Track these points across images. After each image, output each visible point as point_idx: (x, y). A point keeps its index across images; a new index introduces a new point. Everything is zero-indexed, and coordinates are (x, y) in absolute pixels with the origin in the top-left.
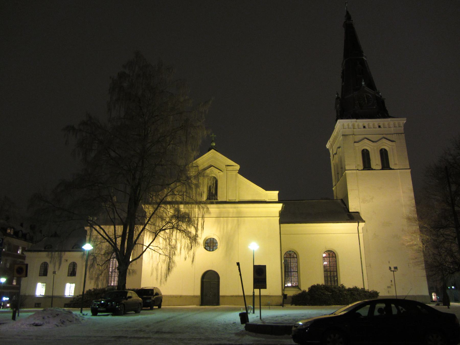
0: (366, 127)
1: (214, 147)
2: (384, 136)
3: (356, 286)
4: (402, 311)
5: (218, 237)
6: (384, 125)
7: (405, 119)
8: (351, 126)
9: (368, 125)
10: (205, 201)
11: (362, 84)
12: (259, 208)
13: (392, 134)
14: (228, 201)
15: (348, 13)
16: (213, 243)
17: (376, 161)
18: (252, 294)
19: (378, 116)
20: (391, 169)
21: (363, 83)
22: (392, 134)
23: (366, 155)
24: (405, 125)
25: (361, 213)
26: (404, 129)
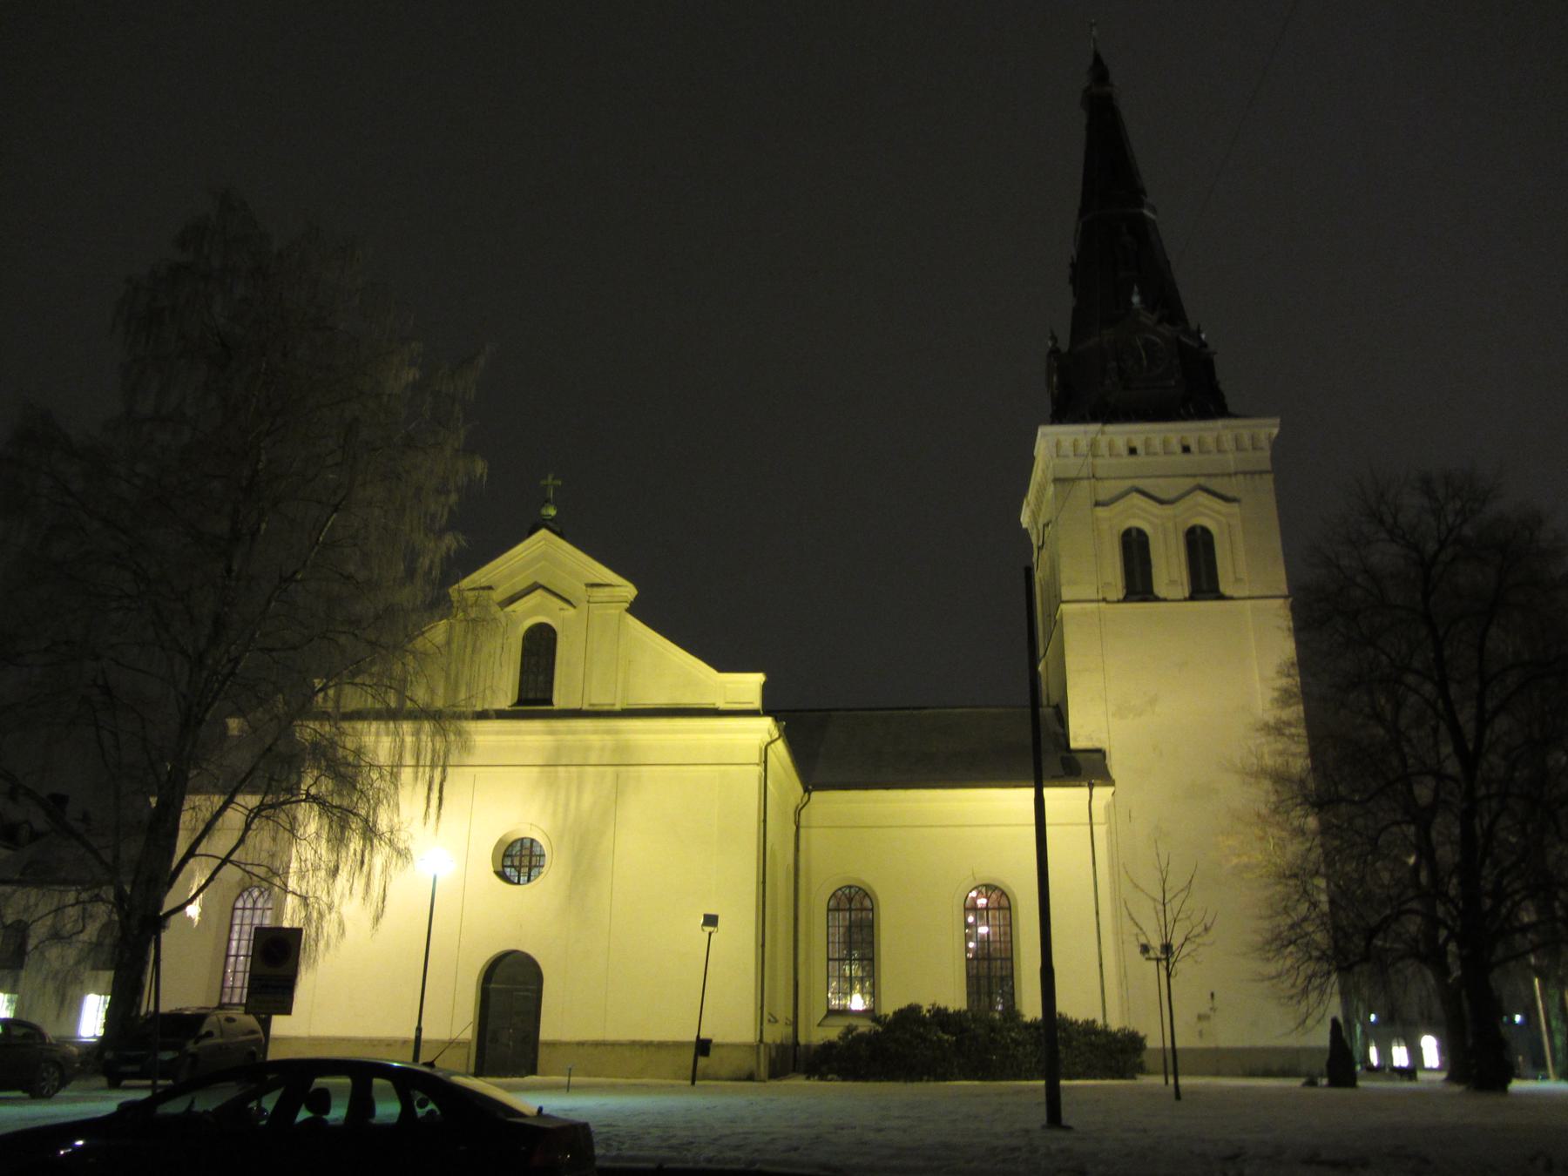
0: (1194, 447)
1: (551, 520)
2: (1202, 481)
4: (420, 1112)
5: (545, 834)
6: (1200, 442)
7: (1277, 421)
8: (1085, 448)
9: (1147, 443)
10: (510, 709)
11: (1131, 303)
12: (689, 731)
13: (1229, 475)
14: (585, 707)
15: (1098, 59)
16: (531, 855)
17: (1170, 569)
18: (412, 1035)
19: (1182, 411)
20: (1221, 597)
21: (1136, 299)
22: (1229, 475)
23: (1135, 548)
24: (1277, 445)
25: (1110, 752)
26: (1273, 459)
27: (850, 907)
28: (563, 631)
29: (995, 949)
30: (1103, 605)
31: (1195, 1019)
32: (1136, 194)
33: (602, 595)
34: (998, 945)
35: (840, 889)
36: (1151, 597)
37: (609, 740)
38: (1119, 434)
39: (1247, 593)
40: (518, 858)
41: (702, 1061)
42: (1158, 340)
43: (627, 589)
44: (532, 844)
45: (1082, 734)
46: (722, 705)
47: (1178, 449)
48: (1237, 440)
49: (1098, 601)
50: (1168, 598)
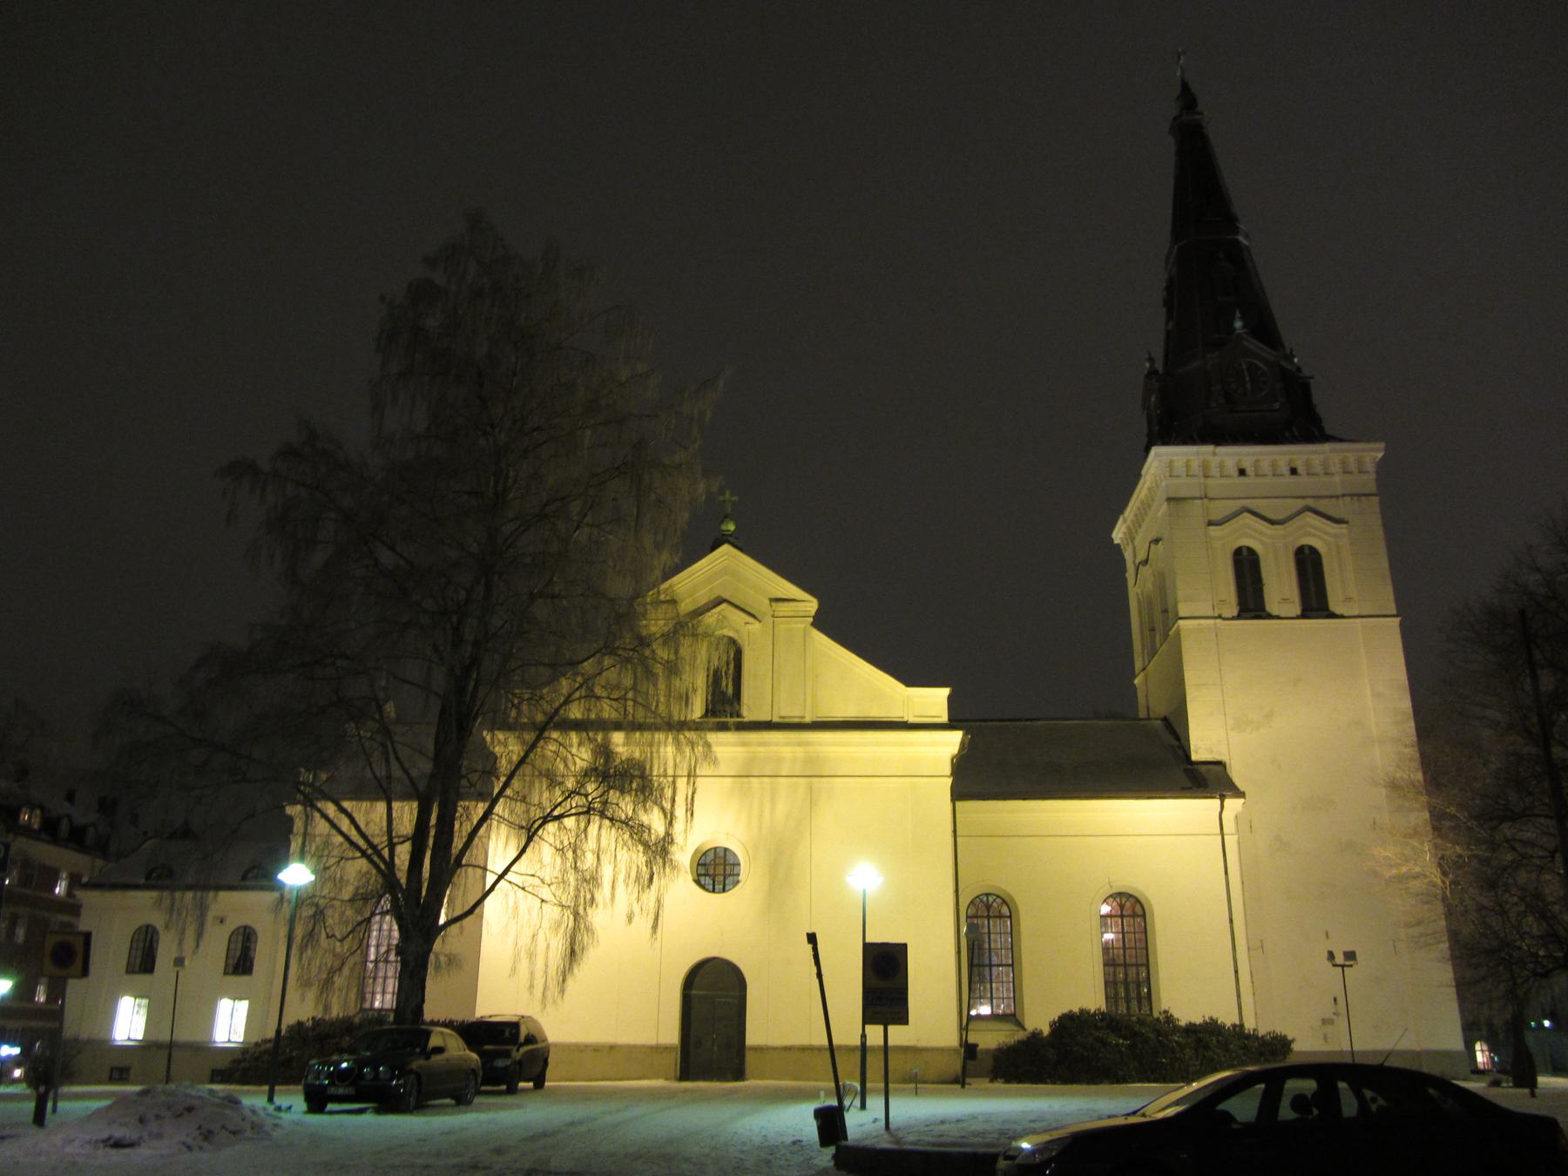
1: (730, 535)
2: (1310, 502)
3: (1214, 1017)
4: (1374, 1107)
7: (1382, 445)
13: (1337, 497)
14: (776, 719)
15: (1185, 87)
17: (1281, 587)
18: (858, 1042)
20: (1333, 616)
21: (1238, 324)
22: (1337, 497)
23: (1246, 566)
24: (1382, 467)
27: (1124, 916)
28: (749, 645)
29: (1131, 956)
30: (1219, 621)
31: (1320, 1023)
32: (1231, 222)
33: (786, 609)
34: (1134, 951)
35: (978, 897)
36: (1263, 614)
37: (799, 751)
38: (1230, 456)
39: (1356, 613)
40: (712, 867)
41: (970, 1063)
42: (1262, 365)
43: (811, 604)
44: (725, 854)
45: (1204, 742)
46: (912, 720)
47: (1286, 471)
48: (1344, 463)
49: (1215, 618)
50: (1282, 615)
